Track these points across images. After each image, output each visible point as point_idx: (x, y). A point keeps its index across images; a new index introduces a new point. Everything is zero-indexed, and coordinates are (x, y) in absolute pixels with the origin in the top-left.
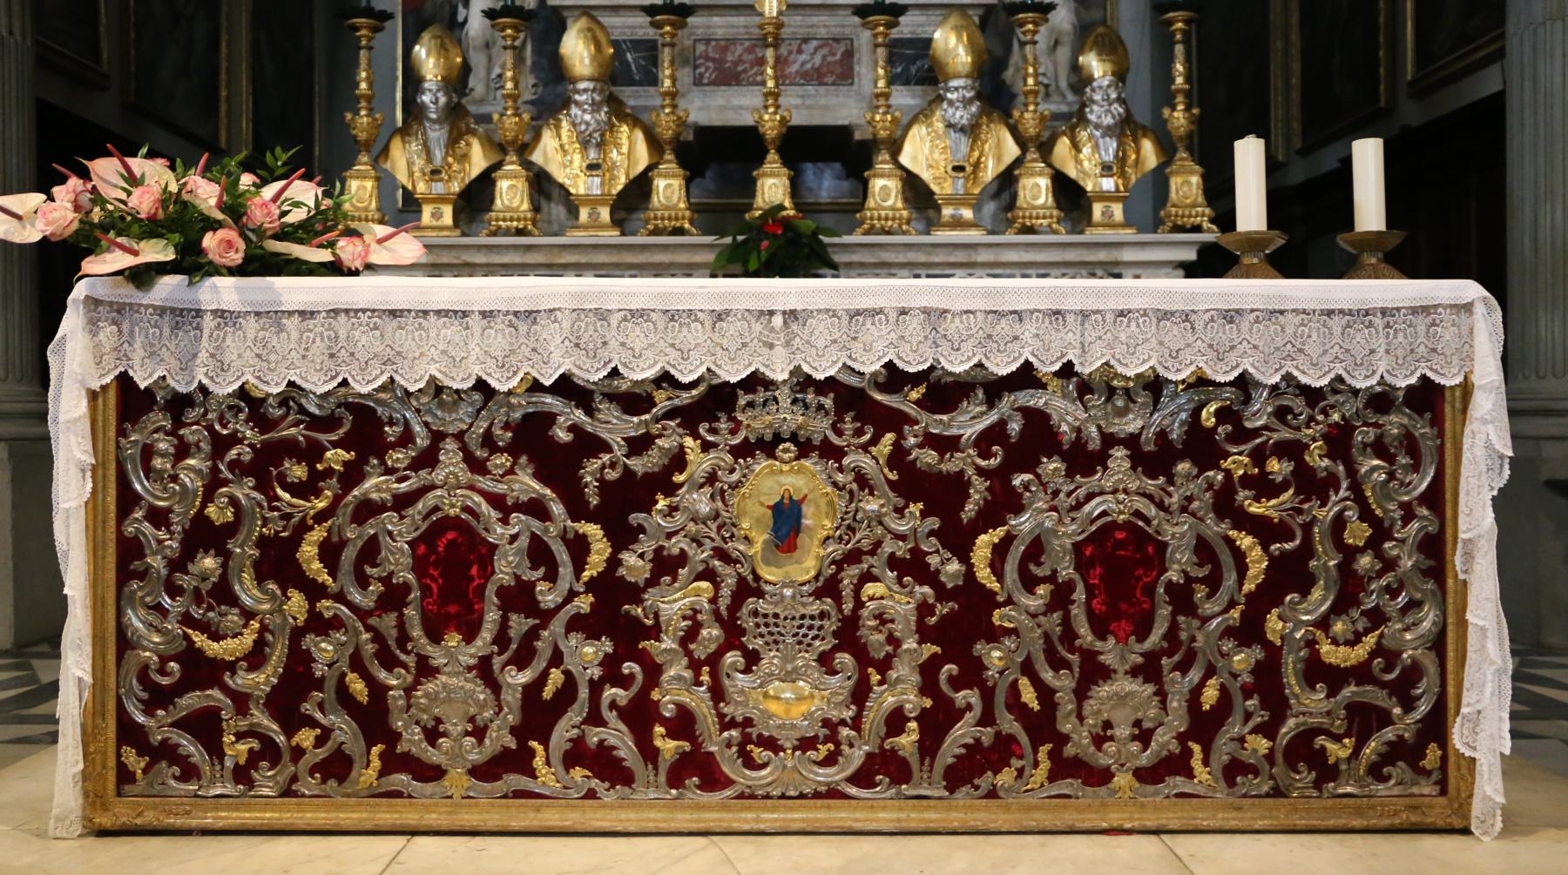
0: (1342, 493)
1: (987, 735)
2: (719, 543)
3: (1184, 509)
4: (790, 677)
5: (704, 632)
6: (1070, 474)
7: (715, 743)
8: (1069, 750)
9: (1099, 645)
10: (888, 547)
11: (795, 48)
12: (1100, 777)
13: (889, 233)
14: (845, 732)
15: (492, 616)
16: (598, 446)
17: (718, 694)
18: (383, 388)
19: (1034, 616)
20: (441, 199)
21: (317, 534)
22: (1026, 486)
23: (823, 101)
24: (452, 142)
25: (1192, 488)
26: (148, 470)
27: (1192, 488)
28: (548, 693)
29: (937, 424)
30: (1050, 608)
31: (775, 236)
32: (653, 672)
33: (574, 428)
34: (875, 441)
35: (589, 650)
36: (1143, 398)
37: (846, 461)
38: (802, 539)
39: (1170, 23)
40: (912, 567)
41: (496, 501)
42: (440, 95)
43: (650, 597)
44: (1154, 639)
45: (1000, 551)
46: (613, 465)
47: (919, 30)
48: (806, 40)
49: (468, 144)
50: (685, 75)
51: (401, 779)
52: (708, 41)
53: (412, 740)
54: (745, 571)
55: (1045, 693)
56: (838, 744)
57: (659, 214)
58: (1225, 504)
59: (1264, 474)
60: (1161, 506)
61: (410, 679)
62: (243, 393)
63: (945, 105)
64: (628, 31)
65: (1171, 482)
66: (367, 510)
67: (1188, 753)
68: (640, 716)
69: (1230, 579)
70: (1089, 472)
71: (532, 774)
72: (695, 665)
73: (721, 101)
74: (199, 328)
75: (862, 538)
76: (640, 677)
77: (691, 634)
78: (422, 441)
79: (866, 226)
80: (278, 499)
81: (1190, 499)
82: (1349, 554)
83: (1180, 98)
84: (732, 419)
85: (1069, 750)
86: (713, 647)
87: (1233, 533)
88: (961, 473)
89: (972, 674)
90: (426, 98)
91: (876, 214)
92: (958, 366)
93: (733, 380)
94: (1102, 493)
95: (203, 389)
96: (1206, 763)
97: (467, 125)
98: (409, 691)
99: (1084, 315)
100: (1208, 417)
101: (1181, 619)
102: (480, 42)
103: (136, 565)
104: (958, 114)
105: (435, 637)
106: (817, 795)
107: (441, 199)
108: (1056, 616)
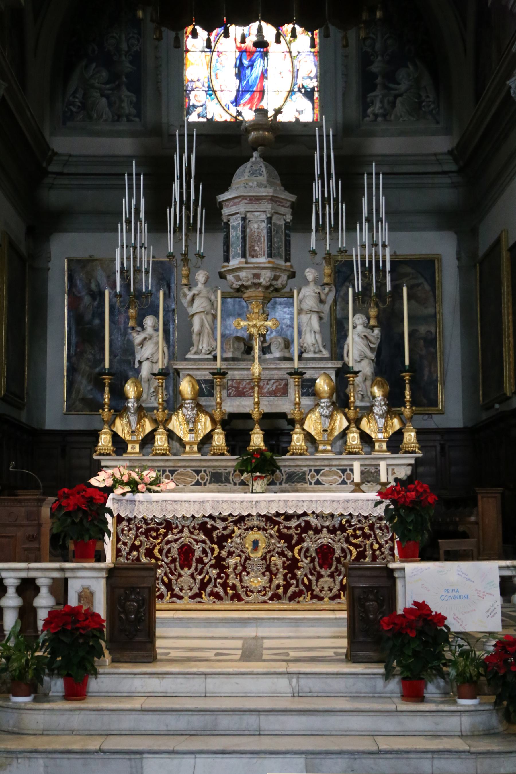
0: (372, 538)
1: (297, 590)
2: (241, 549)
3: (339, 542)
4: (256, 577)
5: (238, 568)
6: (314, 534)
7: (240, 591)
8: (315, 593)
9: (321, 570)
10: (276, 550)
11: (266, 383)
12: (321, 599)
13: (301, 454)
14: (267, 589)
15: (194, 564)
16: (217, 529)
17: (241, 581)
18: (172, 517)
19: (307, 564)
20: (134, 442)
21: (158, 547)
22: (305, 537)
23: (276, 403)
24: (139, 420)
25: (340, 537)
26: (123, 534)
27: (340, 537)
28: (205, 580)
29: (287, 524)
30: (311, 562)
31: (257, 458)
32: (228, 576)
33: (212, 525)
34: (274, 527)
35: (214, 572)
36: (330, 518)
37: (268, 532)
38: (259, 548)
39: (404, 376)
40: (282, 554)
41: (195, 540)
42: (135, 404)
43: (227, 560)
44: (333, 569)
45: (300, 550)
46: (220, 533)
47: (313, 376)
48: (270, 380)
49: (145, 422)
50: (224, 393)
51: (175, 599)
52: (233, 380)
53: (177, 590)
54: (247, 555)
55: (309, 580)
56: (266, 591)
57: (215, 448)
58: (347, 541)
59: (356, 534)
60: (334, 541)
61: (177, 578)
62: (143, 518)
63: (320, 407)
64: (203, 377)
65: (336, 535)
66: (168, 542)
67: (340, 594)
68: (225, 586)
69: (349, 557)
70: (318, 534)
71: (202, 598)
72: (236, 575)
73: (238, 403)
74: (135, 504)
75: (271, 548)
76: (225, 577)
77: (235, 568)
78: (180, 528)
79: (291, 452)
80: (150, 540)
81: (340, 539)
82: (374, 551)
83: (408, 404)
84: (244, 523)
85: (315, 593)
86: (240, 571)
87: (349, 547)
88: (292, 534)
89: (294, 577)
90: (130, 405)
91: (294, 448)
92: (291, 512)
93: (245, 515)
94: (321, 538)
95: (135, 517)
96: (344, 596)
97: (144, 414)
98: (176, 580)
99: (317, 501)
100: (344, 522)
101: (338, 565)
102: (146, 379)
103: (120, 554)
104: (325, 411)
105: (182, 569)
106: (262, 603)
107: (134, 442)
108: (312, 564)
